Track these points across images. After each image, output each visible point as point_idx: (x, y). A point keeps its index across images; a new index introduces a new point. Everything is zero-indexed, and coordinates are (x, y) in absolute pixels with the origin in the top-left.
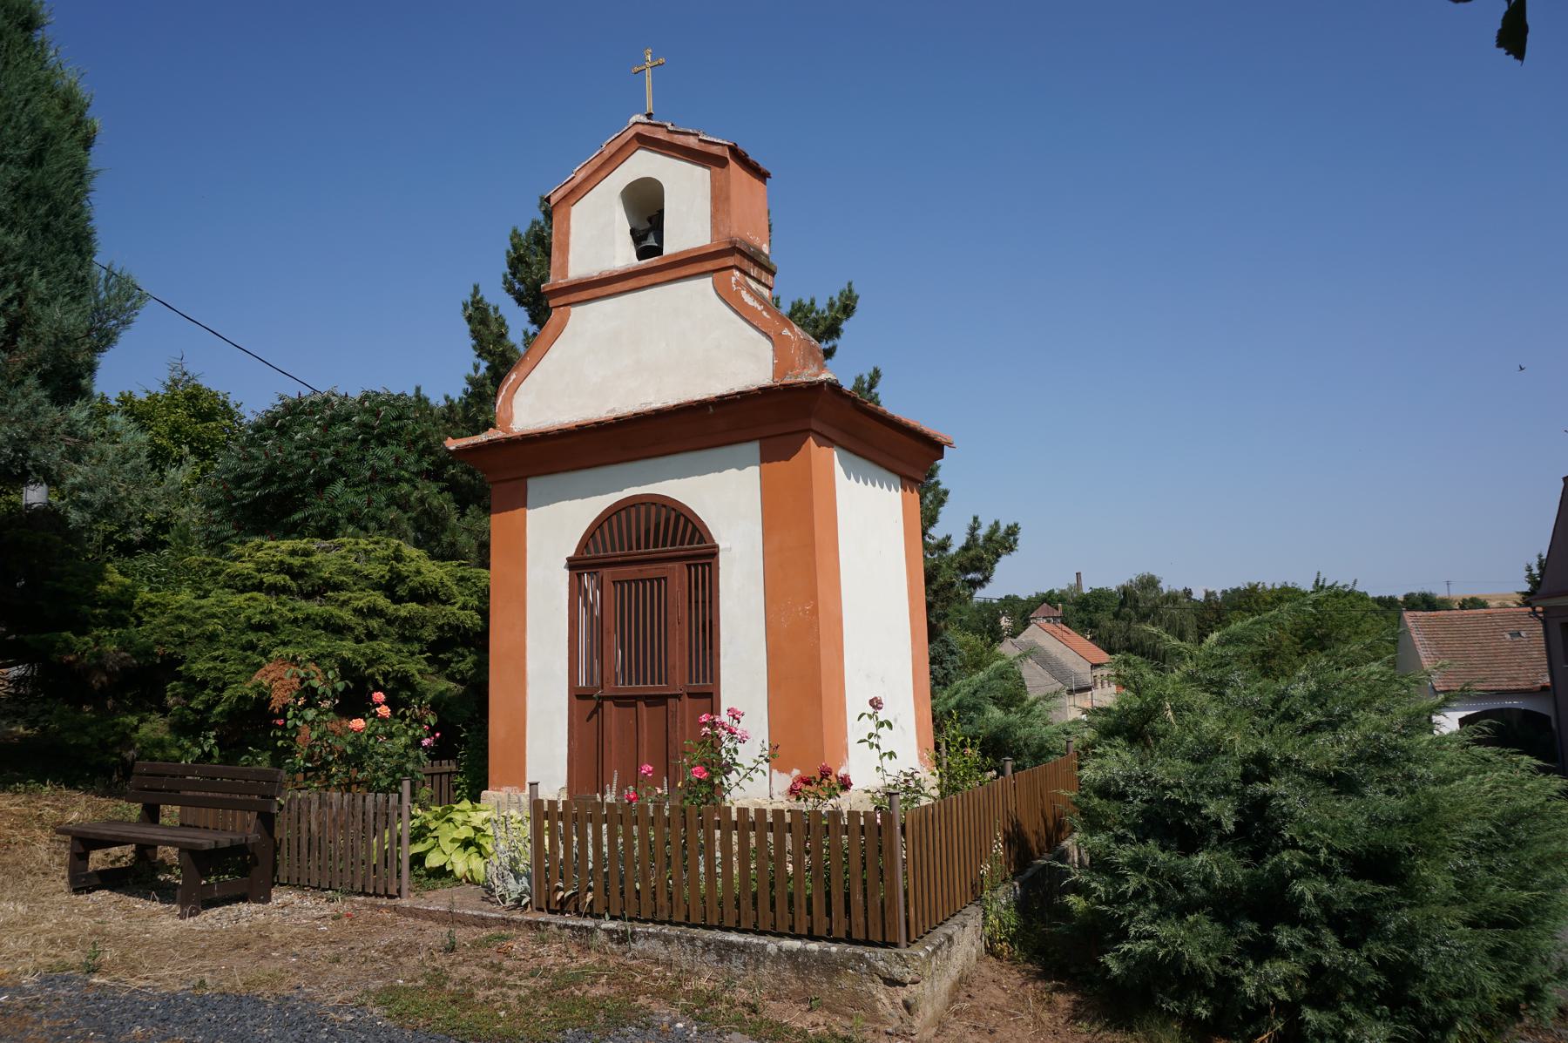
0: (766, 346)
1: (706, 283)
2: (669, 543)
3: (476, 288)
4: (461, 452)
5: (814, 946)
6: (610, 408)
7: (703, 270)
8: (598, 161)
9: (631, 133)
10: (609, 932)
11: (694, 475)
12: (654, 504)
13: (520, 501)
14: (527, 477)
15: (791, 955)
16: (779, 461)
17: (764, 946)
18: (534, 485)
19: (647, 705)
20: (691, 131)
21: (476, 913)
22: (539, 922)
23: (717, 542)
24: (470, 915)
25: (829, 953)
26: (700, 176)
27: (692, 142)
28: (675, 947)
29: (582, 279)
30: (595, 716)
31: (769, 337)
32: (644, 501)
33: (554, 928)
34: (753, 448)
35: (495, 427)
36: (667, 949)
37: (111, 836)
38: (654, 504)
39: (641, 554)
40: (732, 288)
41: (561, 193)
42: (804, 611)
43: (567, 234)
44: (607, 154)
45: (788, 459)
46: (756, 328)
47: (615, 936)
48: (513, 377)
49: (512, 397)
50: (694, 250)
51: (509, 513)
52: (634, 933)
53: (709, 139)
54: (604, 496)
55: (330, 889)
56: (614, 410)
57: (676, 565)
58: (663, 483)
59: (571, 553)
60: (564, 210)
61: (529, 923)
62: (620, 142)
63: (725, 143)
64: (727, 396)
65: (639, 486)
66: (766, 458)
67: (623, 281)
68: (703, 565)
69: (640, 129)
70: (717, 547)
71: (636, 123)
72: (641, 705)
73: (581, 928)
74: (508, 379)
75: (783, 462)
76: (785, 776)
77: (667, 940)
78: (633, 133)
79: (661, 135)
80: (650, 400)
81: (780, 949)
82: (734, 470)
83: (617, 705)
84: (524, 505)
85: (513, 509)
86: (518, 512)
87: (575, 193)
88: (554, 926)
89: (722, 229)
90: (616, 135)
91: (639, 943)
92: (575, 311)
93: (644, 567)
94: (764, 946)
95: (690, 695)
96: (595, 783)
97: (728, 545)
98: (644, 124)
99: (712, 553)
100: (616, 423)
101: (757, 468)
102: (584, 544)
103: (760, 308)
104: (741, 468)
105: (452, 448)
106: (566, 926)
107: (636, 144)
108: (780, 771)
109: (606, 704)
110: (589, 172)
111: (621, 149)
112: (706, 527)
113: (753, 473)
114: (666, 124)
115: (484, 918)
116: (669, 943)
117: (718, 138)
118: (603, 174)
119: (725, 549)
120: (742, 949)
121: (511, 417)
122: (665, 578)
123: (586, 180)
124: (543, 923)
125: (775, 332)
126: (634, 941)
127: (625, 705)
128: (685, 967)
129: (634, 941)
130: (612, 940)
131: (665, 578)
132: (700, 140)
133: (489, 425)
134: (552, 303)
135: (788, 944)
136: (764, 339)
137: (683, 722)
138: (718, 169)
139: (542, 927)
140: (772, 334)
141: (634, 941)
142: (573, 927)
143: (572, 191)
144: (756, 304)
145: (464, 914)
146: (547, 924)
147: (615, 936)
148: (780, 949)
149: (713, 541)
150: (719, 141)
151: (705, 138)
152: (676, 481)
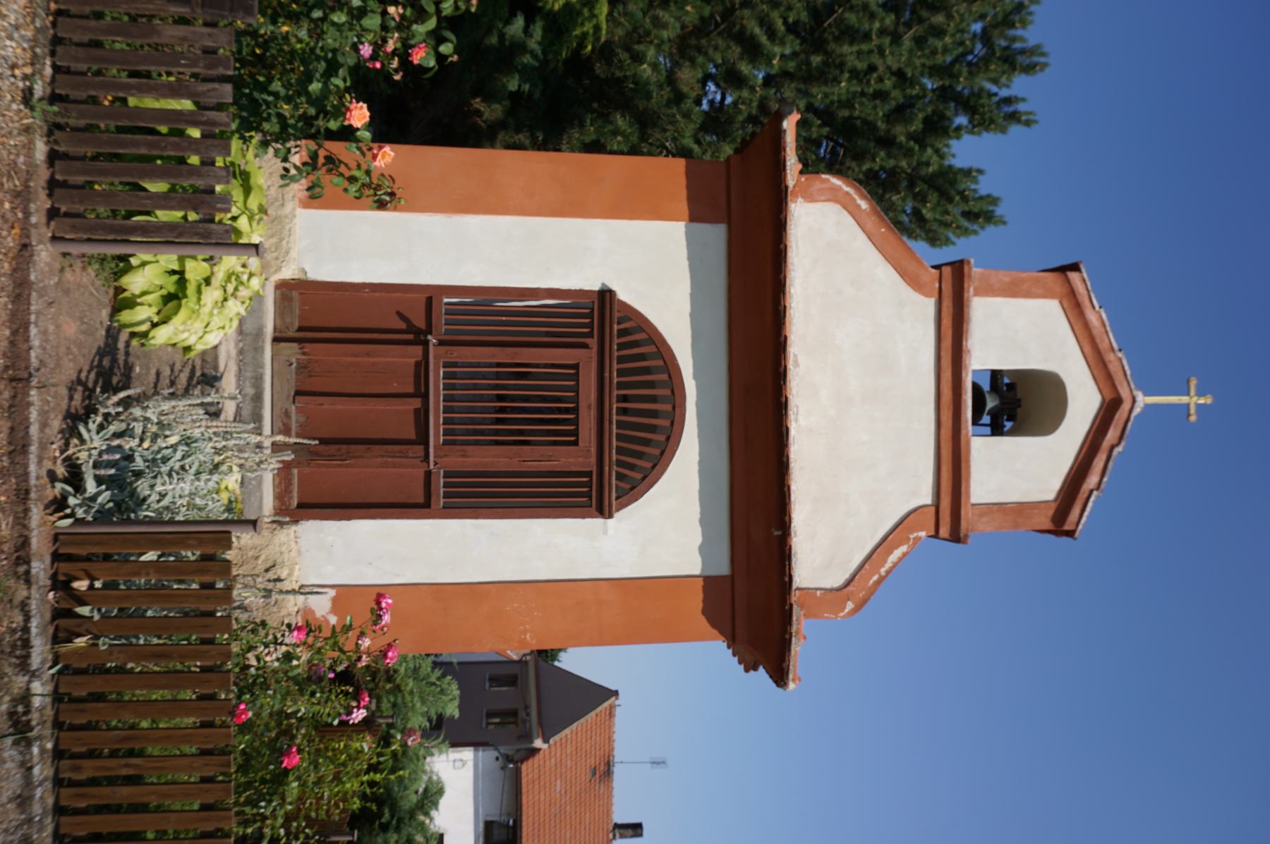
0: (836, 580)
1: (926, 498)
2: (620, 431)
4: (779, 134)
8: (1103, 346)
9: (1125, 393)
10: (25, 698)
12: (674, 408)
14: (729, 221)
16: (704, 601)
18: (716, 235)
19: (417, 411)
20: (1105, 479)
21: (34, 430)
22: (28, 562)
23: (617, 515)
24: (27, 419)
26: (1047, 487)
27: (1092, 480)
29: (968, 324)
30: (403, 326)
31: (848, 583)
32: (677, 409)
33: (22, 593)
34: (722, 567)
35: (801, 172)
36: (10, 801)
38: (674, 408)
40: (913, 532)
41: (1080, 288)
42: (524, 632)
44: (1110, 357)
45: (704, 612)
46: (861, 566)
47: (20, 709)
48: (864, 205)
49: (836, 201)
50: (968, 467)
51: (683, 193)
52: (29, 744)
53: (1090, 504)
55: (56, 68)
56: (796, 364)
57: (593, 460)
58: (697, 440)
59: (623, 295)
62: (1118, 377)
63: (1080, 527)
64: (790, 565)
66: (709, 582)
68: (591, 326)
69: (1126, 406)
70: (610, 516)
71: (1134, 401)
72: (417, 403)
73: (26, 644)
74: (863, 197)
75: (701, 605)
79: (1112, 435)
80: (801, 418)
83: (418, 364)
84: (695, 217)
86: (683, 207)
87: (1074, 309)
88: (25, 593)
89: (984, 519)
90: (1128, 372)
91: (13, 753)
92: (929, 304)
93: (593, 412)
95: (428, 474)
96: (315, 322)
97: (611, 532)
98: (1131, 411)
99: (603, 511)
100: (781, 403)
101: (697, 571)
102: (630, 314)
103: (883, 571)
104: (702, 549)
105: (785, 124)
106: (27, 618)
107: (1109, 396)
108: (335, 600)
109: (418, 350)
110: (1095, 332)
111: (1109, 377)
112: (636, 500)
113: (693, 566)
114: (1123, 444)
115: (24, 449)
116: (19, 805)
117: (1088, 517)
118: (1088, 349)
121: (810, 199)
122: (576, 443)
123: (1086, 325)
124: (28, 572)
125: (852, 592)
126: (16, 743)
127: (417, 376)
129: (16, 743)
130: (15, 701)
131: (576, 443)
132: (1091, 492)
133: (808, 167)
136: (847, 576)
137: (394, 466)
138: (1051, 513)
139: (22, 569)
140: (850, 588)
141: (16, 743)
142: (26, 629)
144: (888, 565)
145: (29, 404)
146: (27, 579)
147: (20, 709)
149: (618, 510)
150: (1084, 519)
151: (1092, 499)
152: (697, 458)
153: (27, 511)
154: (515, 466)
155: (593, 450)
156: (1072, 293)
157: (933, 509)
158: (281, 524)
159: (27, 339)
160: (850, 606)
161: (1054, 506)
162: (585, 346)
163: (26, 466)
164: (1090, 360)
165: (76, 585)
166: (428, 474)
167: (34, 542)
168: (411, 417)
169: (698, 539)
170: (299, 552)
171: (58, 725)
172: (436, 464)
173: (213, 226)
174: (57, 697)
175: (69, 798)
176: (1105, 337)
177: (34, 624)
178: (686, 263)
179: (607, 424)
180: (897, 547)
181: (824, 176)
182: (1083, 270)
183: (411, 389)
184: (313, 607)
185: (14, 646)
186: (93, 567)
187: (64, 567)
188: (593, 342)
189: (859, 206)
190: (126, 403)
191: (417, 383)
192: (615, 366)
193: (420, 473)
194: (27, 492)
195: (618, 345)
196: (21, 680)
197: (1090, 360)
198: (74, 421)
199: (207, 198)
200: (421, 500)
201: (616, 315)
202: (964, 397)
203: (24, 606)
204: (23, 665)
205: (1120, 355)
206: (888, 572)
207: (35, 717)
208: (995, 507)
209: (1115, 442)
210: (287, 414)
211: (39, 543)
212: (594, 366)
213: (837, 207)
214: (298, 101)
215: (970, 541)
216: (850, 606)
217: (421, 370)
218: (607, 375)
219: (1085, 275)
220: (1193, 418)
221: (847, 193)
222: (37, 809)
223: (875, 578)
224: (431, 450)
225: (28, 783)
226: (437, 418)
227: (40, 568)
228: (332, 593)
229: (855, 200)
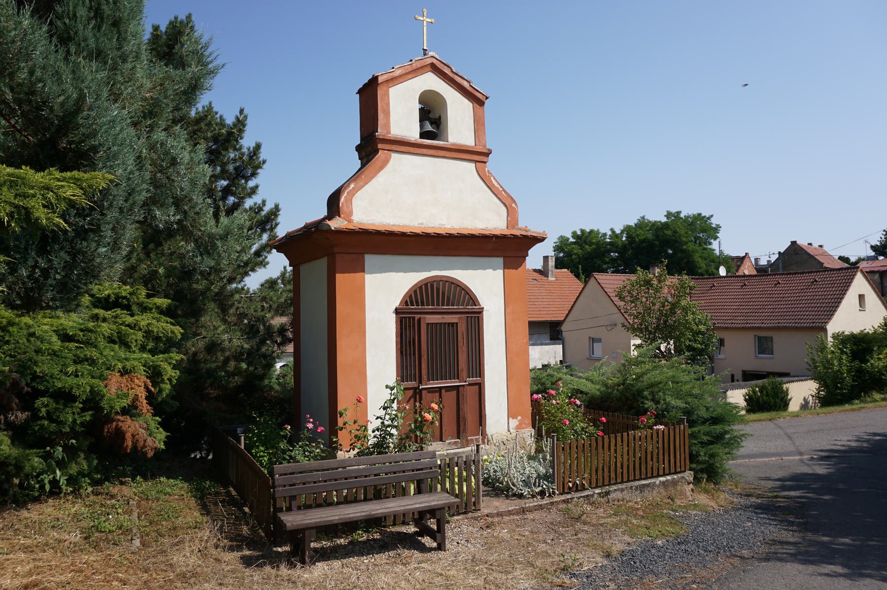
3: (712, 216)
5: (669, 478)
6: (420, 222)
7: (453, 156)
9: (429, 61)
10: (599, 494)
11: (470, 269)
13: (360, 268)
14: (363, 254)
15: (663, 483)
17: (655, 483)
25: (674, 479)
27: (466, 84)
28: (626, 492)
29: (404, 139)
33: (575, 499)
34: (500, 261)
37: (365, 516)
39: (444, 309)
43: (388, 104)
45: (517, 269)
46: (499, 199)
50: (463, 146)
54: (419, 273)
56: (422, 224)
57: (462, 316)
60: (385, 88)
61: (563, 501)
65: (441, 270)
66: (506, 266)
67: (417, 148)
68: (409, 318)
69: (435, 61)
71: (433, 57)
73: (587, 496)
76: (515, 420)
77: (622, 490)
78: (430, 62)
81: (660, 482)
82: (491, 270)
84: (363, 270)
85: (355, 272)
86: (358, 275)
92: (395, 156)
93: (445, 316)
94: (655, 483)
99: (480, 312)
101: (502, 271)
103: (501, 189)
106: (581, 497)
107: (429, 68)
108: (513, 418)
109: (424, 392)
110: (404, 72)
111: (422, 67)
115: (541, 505)
118: (410, 76)
119: (486, 310)
120: (647, 485)
123: (401, 76)
124: (571, 499)
125: (509, 204)
127: (433, 392)
128: (628, 499)
132: (470, 86)
134: (380, 146)
135: (662, 479)
136: (502, 205)
138: (478, 106)
139: (570, 501)
142: (584, 497)
143: (392, 79)
144: (499, 187)
148: (660, 482)
149: (480, 305)
153: (556, 502)
154: (465, 349)
155: (459, 316)
156: (387, 81)
157: (477, 163)
158: (488, 441)
159: (513, 510)
160: (513, 205)
161: (475, 104)
162: (419, 320)
163: (545, 504)
164: (414, 76)
165: (571, 486)
166: (470, 385)
167: (563, 498)
168: (448, 393)
169: (491, 270)
170: (497, 433)
171: (604, 485)
172: (465, 382)
173: (442, 465)
174: (597, 487)
175: (619, 480)
176: (406, 67)
177: (582, 495)
178: (383, 274)
179: (449, 310)
180: (492, 182)
181: (340, 205)
182: (377, 74)
183: (438, 394)
184: (515, 426)
185: (588, 499)
186: (566, 481)
187: (566, 491)
188: (417, 317)
189: (353, 188)
190: (514, 485)
191: (435, 392)
192: (440, 307)
193: (468, 387)
194: (551, 503)
195: (411, 306)
196: (596, 496)
197: (414, 76)
198: (521, 496)
199: (468, 463)
200: (478, 386)
201: (405, 307)
202: (434, 145)
203: (579, 498)
204: (592, 496)
205: (414, 61)
206: (501, 187)
207: (603, 491)
208: (476, 134)
209: (450, 69)
210: (449, 444)
211: (563, 497)
212: (427, 316)
213: (354, 200)
214: (265, 463)
215: (490, 148)
216: (513, 205)
217: (431, 390)
218: (430, 311)
219: (380, 74)
220: (433, 20)
221: (348, 193)
222: (624, 487)
223: (503, 193)
224: (462, 384)
225: (618, 490)
226: (455, 382)
227: (569, 496)
228: (510, 419)
229: (350, 190)
